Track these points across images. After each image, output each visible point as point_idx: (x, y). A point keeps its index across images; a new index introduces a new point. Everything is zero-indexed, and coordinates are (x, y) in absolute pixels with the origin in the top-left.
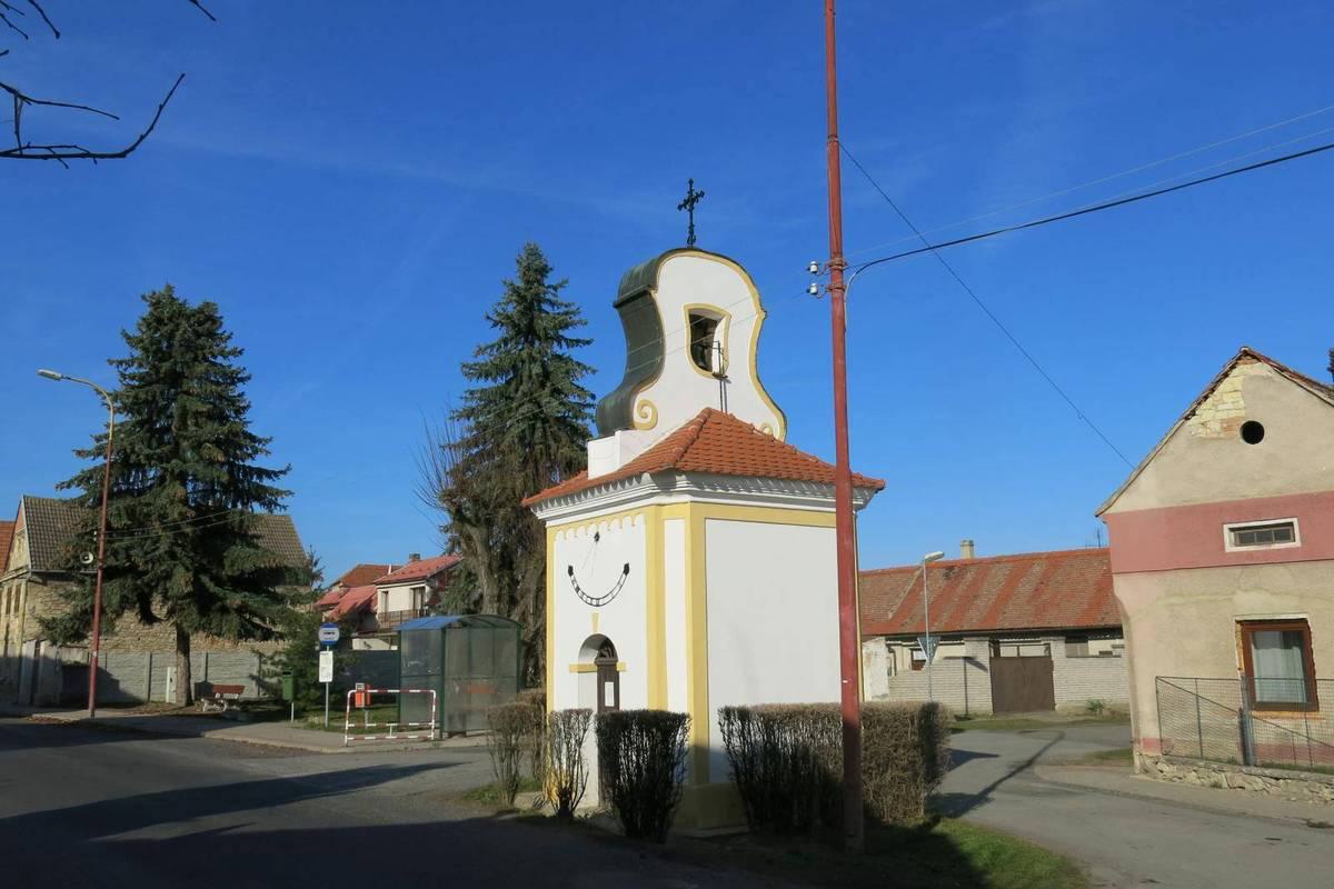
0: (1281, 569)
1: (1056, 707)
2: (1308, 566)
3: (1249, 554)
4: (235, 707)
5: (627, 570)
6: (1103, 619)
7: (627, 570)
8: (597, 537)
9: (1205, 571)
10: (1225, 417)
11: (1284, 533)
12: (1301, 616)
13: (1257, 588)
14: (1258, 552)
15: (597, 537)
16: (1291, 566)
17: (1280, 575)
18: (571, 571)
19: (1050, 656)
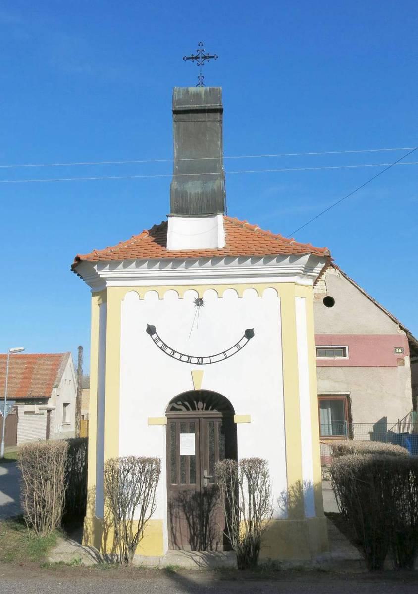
0: (339, 369)
1: (18, 444)
2: (352, 369)
3: (326, 361)
4: (136, 499)
5: (249, 334)
6: (31, 393)
7: (249, 334)
8: (199, 302)
9: (363, 369)
10: (317, 292)
11: (343, 352)
12: (347, 393)
13: (328, 378)
14: (330, 360)
15: (199, 302)
16: (343, 368)
17: (339, 373)
18: (151, 330)
19: (17, 414)
